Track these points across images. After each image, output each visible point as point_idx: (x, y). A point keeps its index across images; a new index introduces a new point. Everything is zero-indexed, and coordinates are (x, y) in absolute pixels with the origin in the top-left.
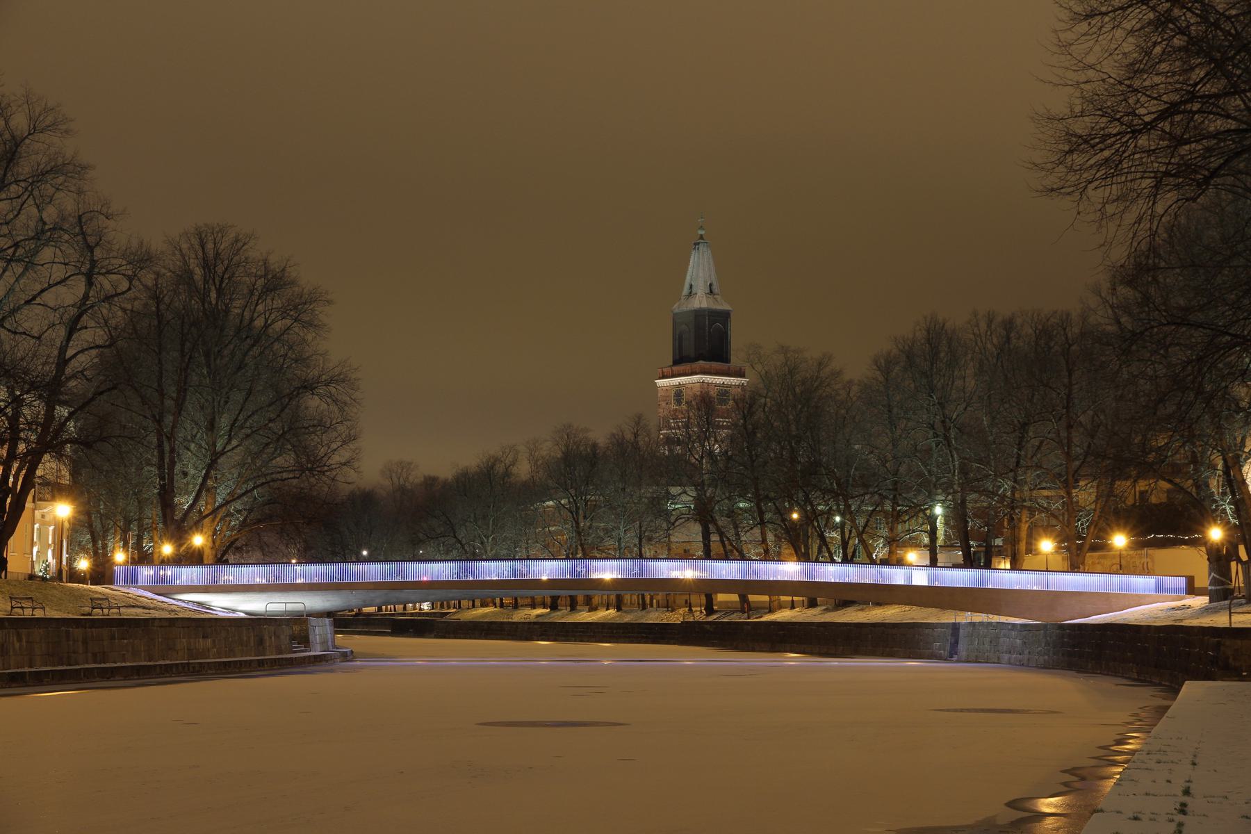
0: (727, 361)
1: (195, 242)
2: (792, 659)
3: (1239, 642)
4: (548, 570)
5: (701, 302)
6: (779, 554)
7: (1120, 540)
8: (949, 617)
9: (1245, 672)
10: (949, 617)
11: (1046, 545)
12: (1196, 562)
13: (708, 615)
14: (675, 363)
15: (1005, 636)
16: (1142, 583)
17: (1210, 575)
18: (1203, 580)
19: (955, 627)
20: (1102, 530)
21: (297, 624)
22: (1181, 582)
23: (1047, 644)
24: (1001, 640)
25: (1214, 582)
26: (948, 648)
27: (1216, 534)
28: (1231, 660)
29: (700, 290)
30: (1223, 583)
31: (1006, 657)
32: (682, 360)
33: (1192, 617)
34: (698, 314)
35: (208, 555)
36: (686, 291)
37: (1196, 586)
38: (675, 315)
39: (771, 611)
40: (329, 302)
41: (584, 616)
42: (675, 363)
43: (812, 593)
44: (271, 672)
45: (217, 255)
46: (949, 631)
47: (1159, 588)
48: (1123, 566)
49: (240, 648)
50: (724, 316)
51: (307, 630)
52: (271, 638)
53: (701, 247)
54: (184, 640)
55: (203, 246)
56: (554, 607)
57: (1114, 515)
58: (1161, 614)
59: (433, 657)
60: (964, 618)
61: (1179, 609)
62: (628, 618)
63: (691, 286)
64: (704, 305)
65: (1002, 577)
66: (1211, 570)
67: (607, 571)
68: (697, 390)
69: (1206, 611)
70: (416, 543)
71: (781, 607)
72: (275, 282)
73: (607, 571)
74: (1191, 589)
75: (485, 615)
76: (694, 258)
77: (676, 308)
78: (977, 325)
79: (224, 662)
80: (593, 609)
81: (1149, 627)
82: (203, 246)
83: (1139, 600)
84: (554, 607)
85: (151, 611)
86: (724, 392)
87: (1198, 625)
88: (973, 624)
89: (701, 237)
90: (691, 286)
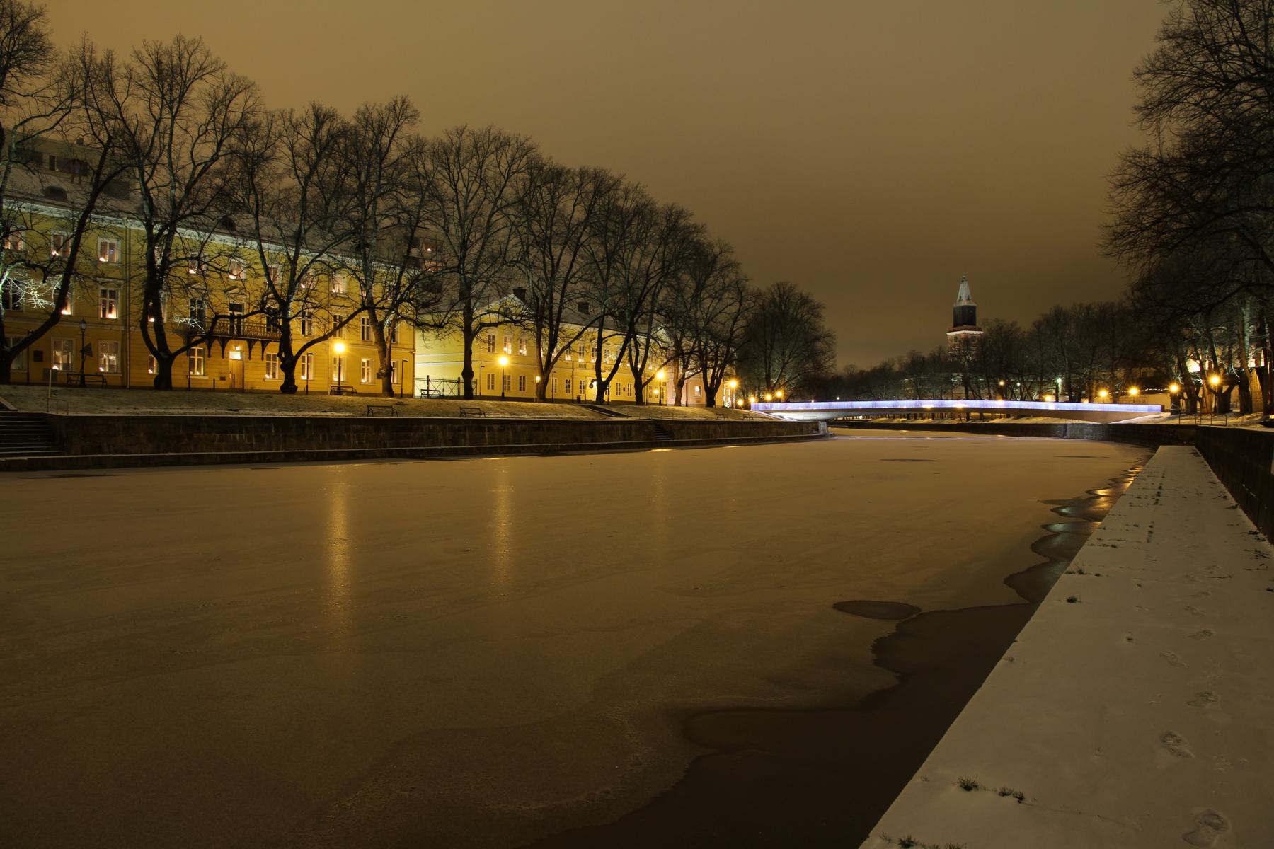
0: (975, 325)
1: (776, 288)
2: (1000, 437)
5: (964, 303)
7: (1134, 391)
8: (1063, 421)
10: (1063, 421)
14: (954, 326)
16: (1142, 408)
18: (1169, 406)
19: (1066, 425)
21: (814, 424)
22: (1159, 407)
29: (964, 298)
30: (1176, 408)
31: (1086, 436)
32: (957, 325)
34: (964, 307)
35: (783, 399)
36: (959, 298)
38: (954, 309)
39: (992, 419)
40: (824, 308)
41: (920, 421)
42: (954, 326)
43: (1008, 412)
45: (784, 292)
46: (1063, 427)
50: (974, 308)
53: (964, 282)
55: (779, 289)
56: (908, 418)
57: (1130, 381)
60: (1069, 422)
62: (936, 422)
63: (960, 297)
64: (966, 304)
65: (1085, 406)
66: (1172, 402)
67: (928, 404)
68: (963, 337)
69: (1169, 418)
70: (857, 395)
72: (805, 301)
73: (928, 404)
74: (1163, 410)
75: (883, 421)
76: (961, 286)
77: (955, 305)
80: (923, 418)
82: (779, 289)
83: (1141, 414)
84: (908, 418)
86: (973, 337)
88: (1073, 424)
89: (964, 278)
90: (960, 297)
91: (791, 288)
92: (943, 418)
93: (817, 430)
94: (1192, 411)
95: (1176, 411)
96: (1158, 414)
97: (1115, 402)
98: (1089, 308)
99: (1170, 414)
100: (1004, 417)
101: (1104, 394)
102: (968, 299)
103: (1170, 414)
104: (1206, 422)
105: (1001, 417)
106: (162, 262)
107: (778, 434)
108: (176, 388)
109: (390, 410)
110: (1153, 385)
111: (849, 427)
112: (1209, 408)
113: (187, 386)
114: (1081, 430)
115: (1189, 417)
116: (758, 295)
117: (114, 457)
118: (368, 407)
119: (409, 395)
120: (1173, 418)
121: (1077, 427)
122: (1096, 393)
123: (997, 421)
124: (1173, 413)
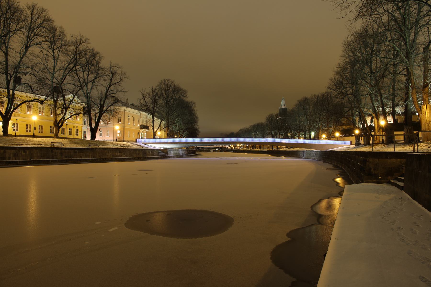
3: (377, 160)
4: (270, 140)
5: (283, 107)
6: (266, 137)
7: (337, 134)
9: (380, 177)
11: (324, 136)
12: (353, 139)
13: (272, 149)
15: (312, 153)
17: (355, 140)
18: (354, 142)
19: (304, 151)
20: (334, 132)
21: (165, 151)
22: (349, 142)
23: (319, 155)
24: (312, 154)
25: (356, 142)
26: (302, 155)
27: (357, 132)
28: (372, 170)
30: (358, 142)
31: (312, 157)
33: (351, 149)
36: (281, 106)
37: (9, 134)
39: (281, 149)
41: (256, 150)
43: (287, 145)
44: (7, 166)
46: (303, 152)
47: (345, 143)
48: (337, 139)
49: (136, 155)
51: (167, 151)
52: (149, 153)
54: (110, 153)
58: (345, 149)
59: (233, 157)
61: (349, 147)
62: (261, 150)
64: (284, 107)
69: (354, 148)
71: (282, 148)
75: (244, 149)
78: (312, 97)
79: (122, 158)
80: (257, 148)
81: (339, 151)
85: (118, 147)
87: (353, 151)
91: (172, 82)
92: (264, 148)
93: (167, 153)
94: (367, 144)
95: (358, 144)
96: (349, 146)
97: (329, 140)
98: (318, 96)
99: (355, 145)
100: (285, 148)
101: (324, 136)
102: (284, 106)
103: (355, 145)
104: (399, 149)
105: (284, 148)
106: (104, 108)
107: (113, 156)
108: (67, 138)
109: (61, 144)
110: (347, 133)
111: (233, 152)
112: (378, 141)
113: (15, 135)
114: (310, 154)
115: (366, 146)
116: (267, 122)
117: (3, 160)
118: (52, 143)
119: (14, 135)
120: (357, 148)
121: (308, 152)
122: (321, 136)
123: (282, 149)
124: (356, 145)
